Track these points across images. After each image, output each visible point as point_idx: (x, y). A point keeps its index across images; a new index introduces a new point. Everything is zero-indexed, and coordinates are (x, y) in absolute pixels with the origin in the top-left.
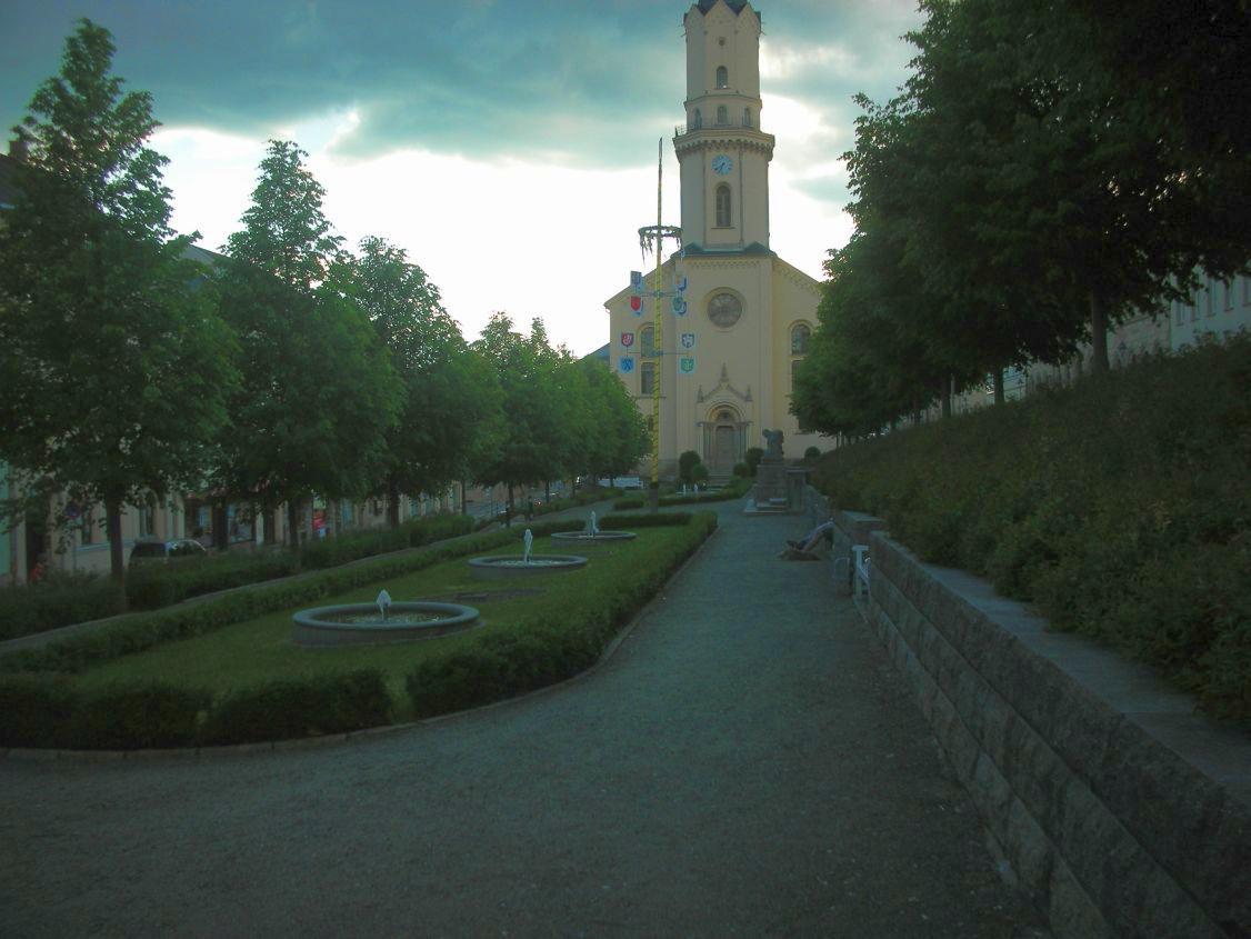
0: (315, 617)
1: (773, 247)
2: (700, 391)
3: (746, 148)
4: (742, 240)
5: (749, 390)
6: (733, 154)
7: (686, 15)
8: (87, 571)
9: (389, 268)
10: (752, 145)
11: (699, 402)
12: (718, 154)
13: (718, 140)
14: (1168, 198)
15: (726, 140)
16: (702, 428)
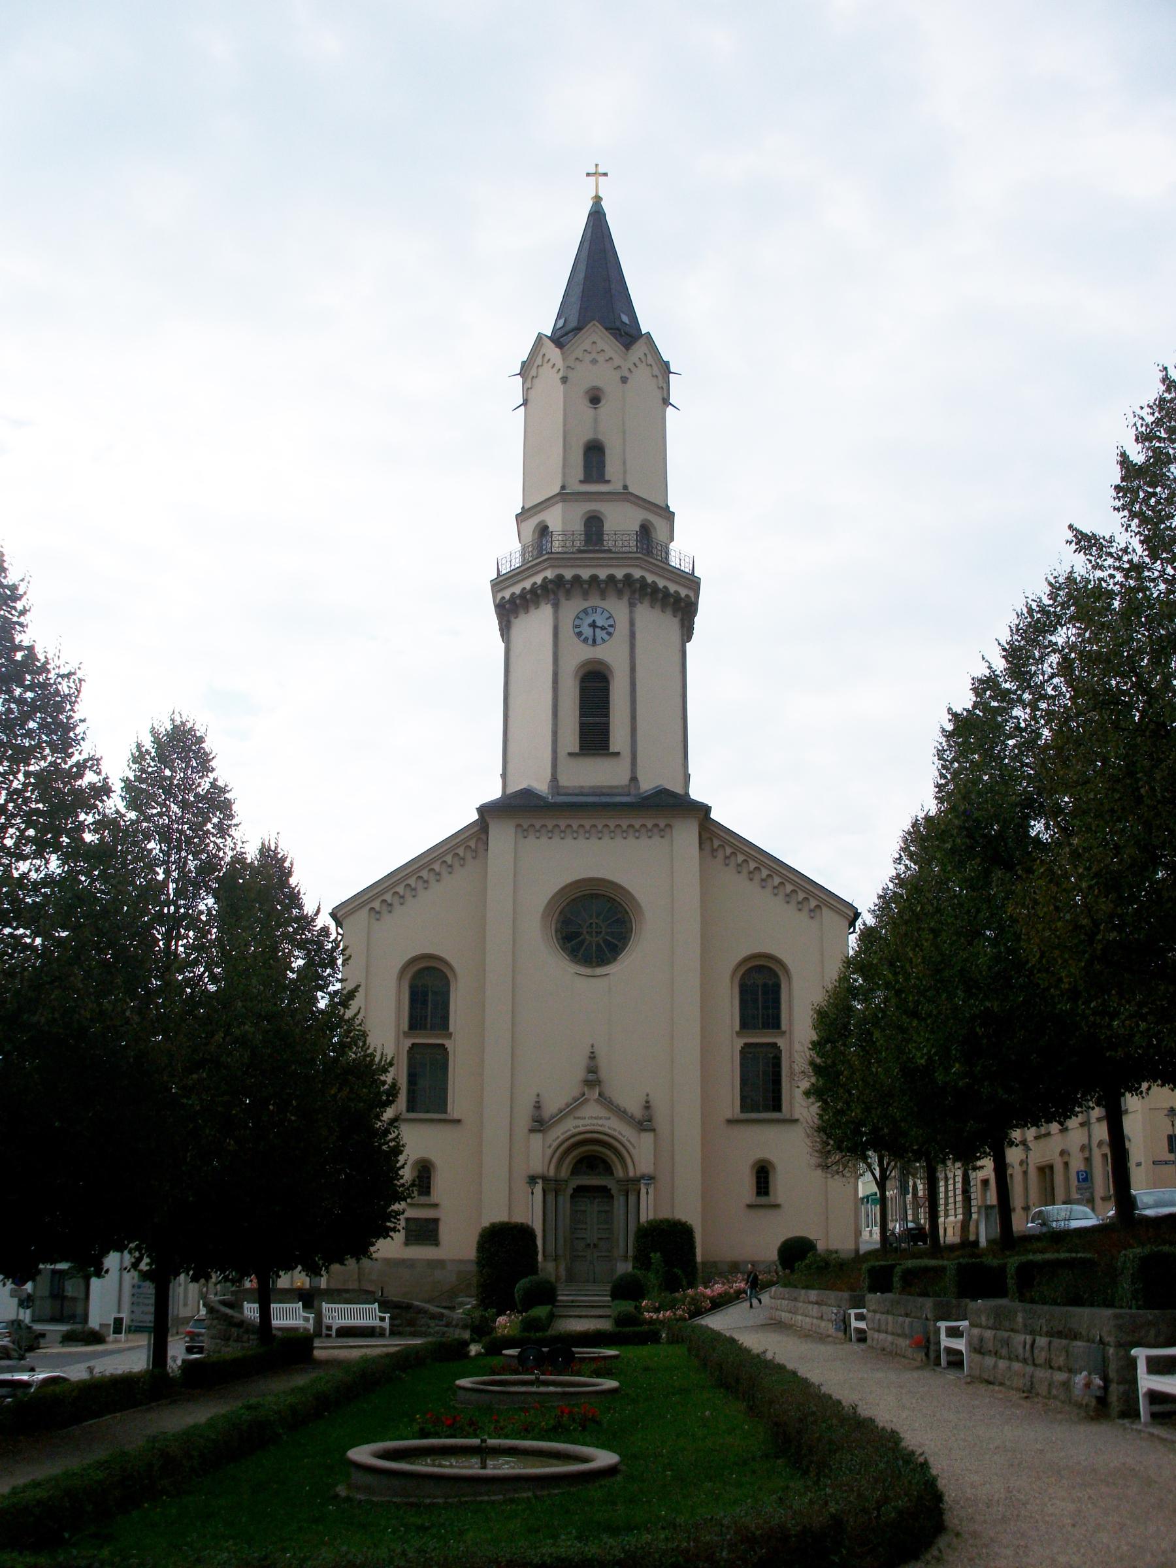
1: (693, 796)
2: (538, 1106)
4: (634, 779)
6: (617, 609)
8: (910, 1448)
9: (184, 732)
10: (655, 589)
11: (532, 1131)
12: (586, 604)
13: (603, 574)
14: (224, 989)
16: (538, 1189)
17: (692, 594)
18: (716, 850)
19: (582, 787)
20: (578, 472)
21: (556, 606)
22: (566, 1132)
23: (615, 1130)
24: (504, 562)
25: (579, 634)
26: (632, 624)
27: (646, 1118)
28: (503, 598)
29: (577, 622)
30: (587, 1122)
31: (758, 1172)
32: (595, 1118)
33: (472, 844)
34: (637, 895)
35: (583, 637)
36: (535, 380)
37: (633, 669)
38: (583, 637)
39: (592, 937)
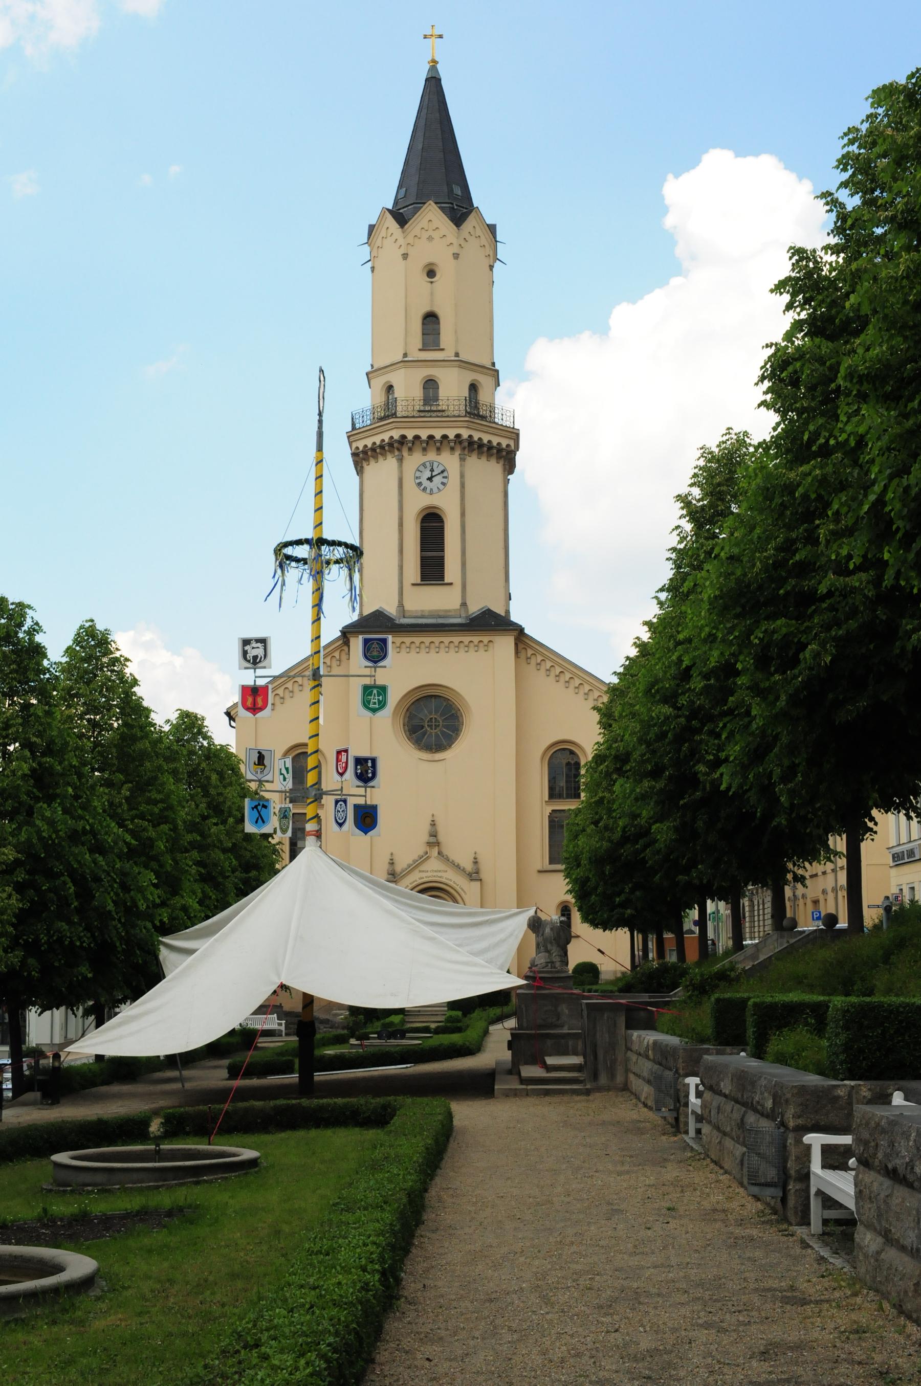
0: (58, 1268)
1: (512, 619)
3: (471, 450)
4: (464, 604)
5: (476, 862)
6: (450, 461)
7: (371, 228)
15: (396, 437)
17: (512, 443)
18: (530, 658)
19: (422, 611)
20: (416, 339)
21: (400, 460)
22: (414, 882)
23: (451, 880)
24: (357, 417)
25: (420, 484)
26: (462, 476)
27: (474, 871)
28: (357, 448)
29: (418, 474)
30: (429, 874)
31: (562, 910)
32: (436, 871)
33: (337, 654)
34: (466, 697)
35: (422, 487)
36: (380, 249)
37: (463, 514)
38: (422, 487)
39: (432, 729)
